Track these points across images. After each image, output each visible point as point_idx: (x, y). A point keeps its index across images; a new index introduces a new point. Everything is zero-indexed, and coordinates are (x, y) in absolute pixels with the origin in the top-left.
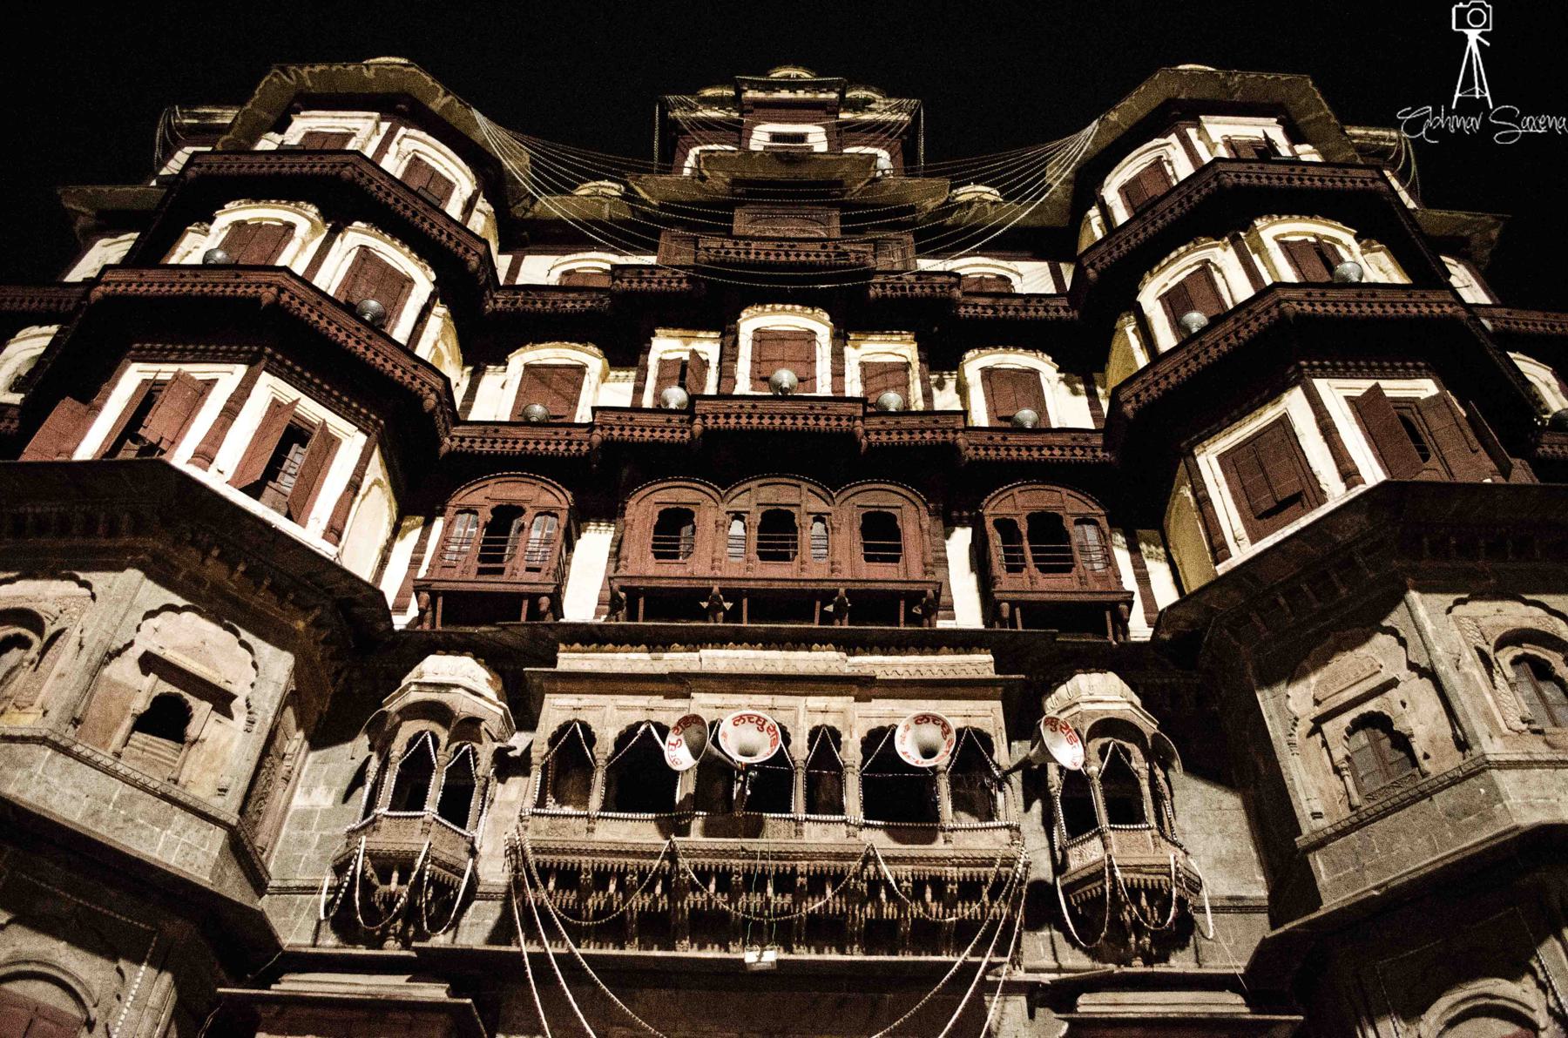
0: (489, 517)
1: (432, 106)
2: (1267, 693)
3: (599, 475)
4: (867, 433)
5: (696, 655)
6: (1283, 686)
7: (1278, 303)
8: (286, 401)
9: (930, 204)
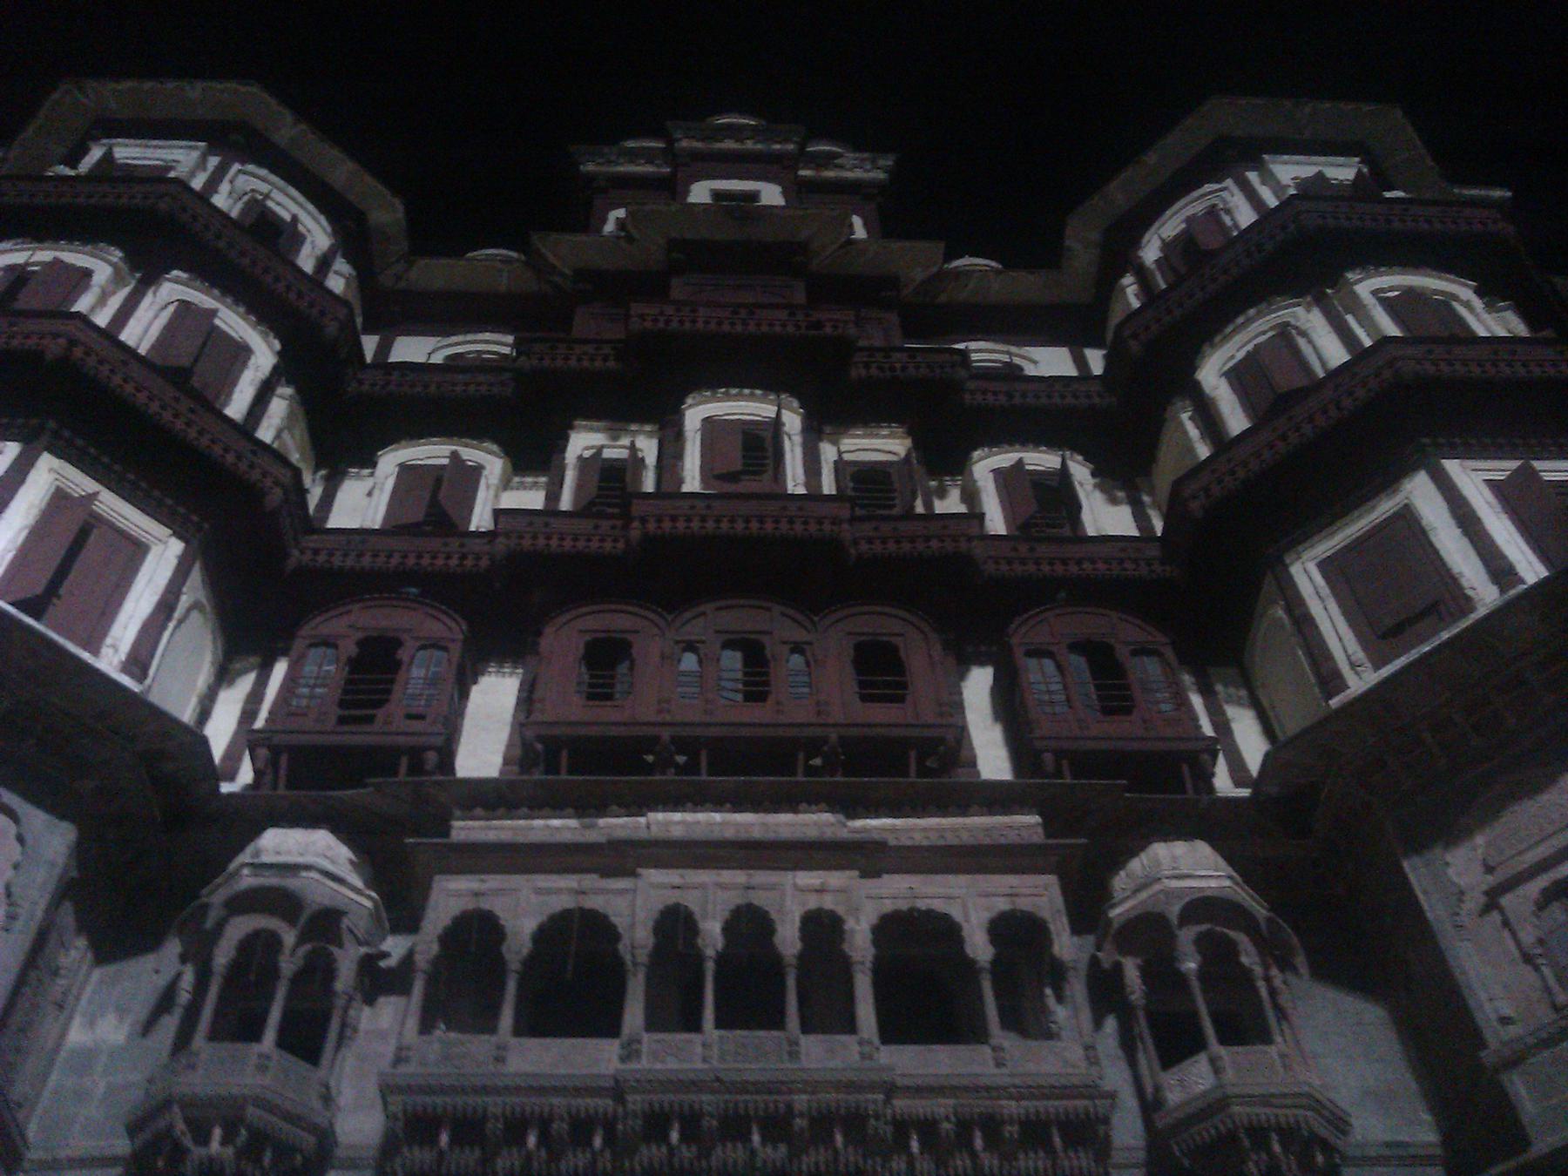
1: (276, 138)
2: (1416, 860)
3: (503, 598)
4: (856, 542)
5: (642, 820)
6: (1438, 851)
7: (1390, 364)
8: (77, 492)
9: (919, 275)
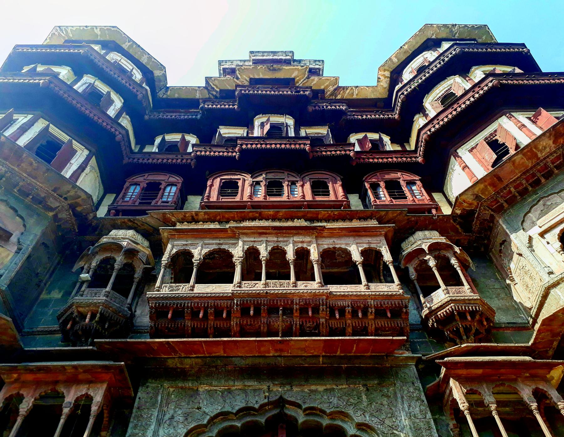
0: (145, 185)
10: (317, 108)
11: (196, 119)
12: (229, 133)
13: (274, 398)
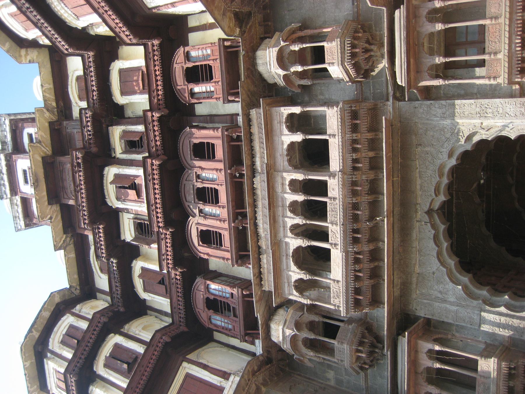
10: (92, 141)
11: (117, 263)
12: (130, 231)
13: (426, 218)
